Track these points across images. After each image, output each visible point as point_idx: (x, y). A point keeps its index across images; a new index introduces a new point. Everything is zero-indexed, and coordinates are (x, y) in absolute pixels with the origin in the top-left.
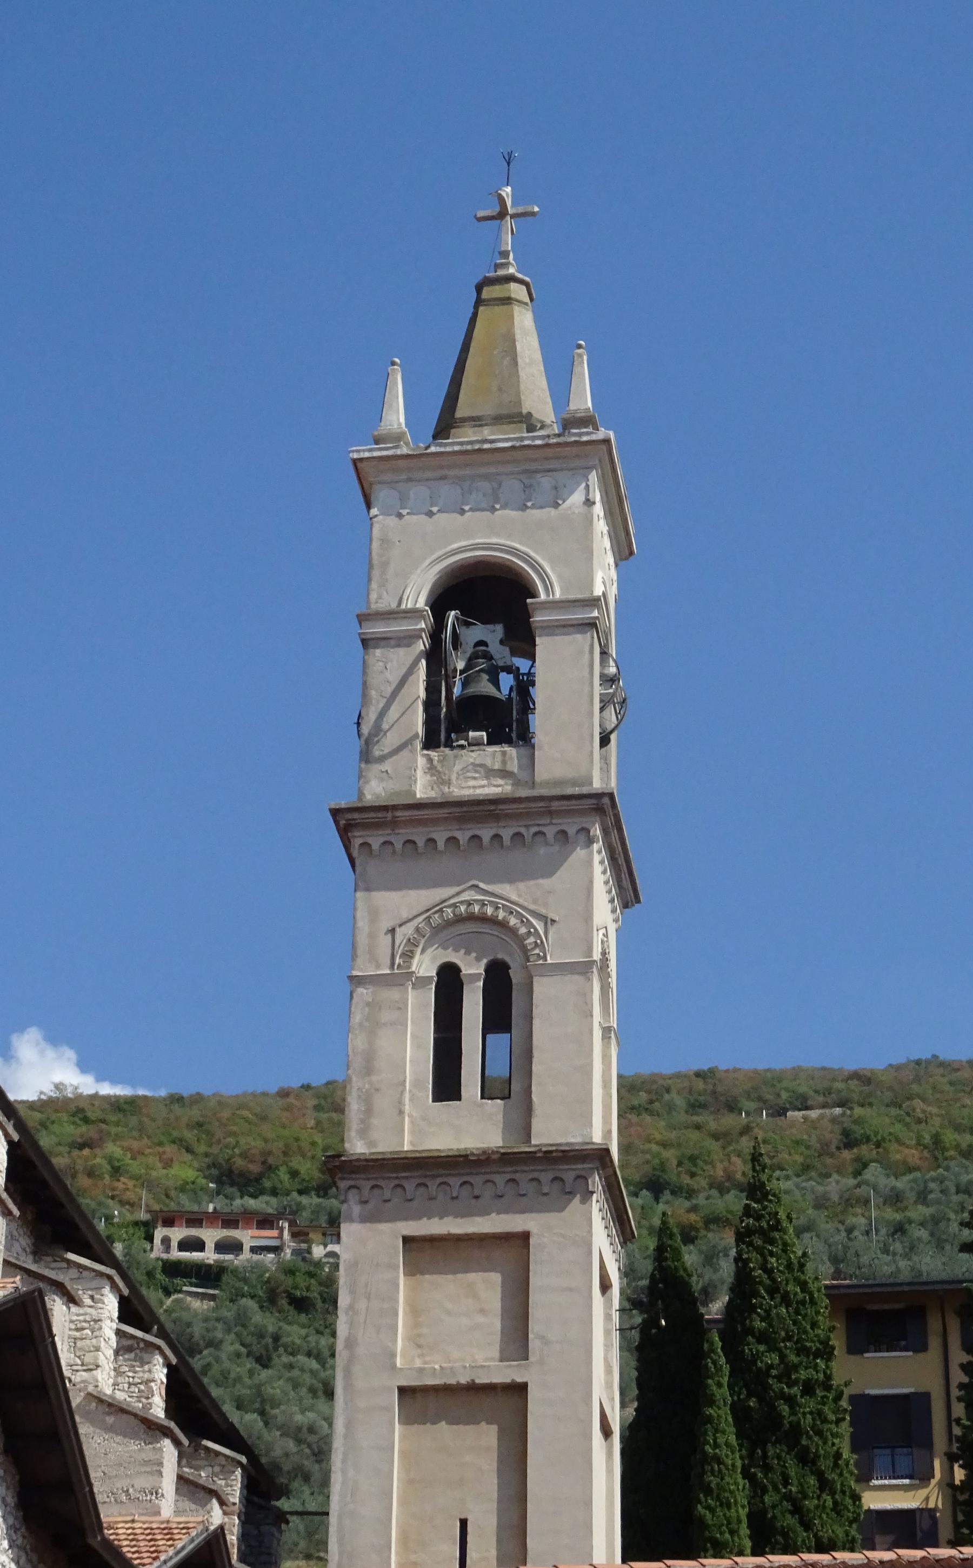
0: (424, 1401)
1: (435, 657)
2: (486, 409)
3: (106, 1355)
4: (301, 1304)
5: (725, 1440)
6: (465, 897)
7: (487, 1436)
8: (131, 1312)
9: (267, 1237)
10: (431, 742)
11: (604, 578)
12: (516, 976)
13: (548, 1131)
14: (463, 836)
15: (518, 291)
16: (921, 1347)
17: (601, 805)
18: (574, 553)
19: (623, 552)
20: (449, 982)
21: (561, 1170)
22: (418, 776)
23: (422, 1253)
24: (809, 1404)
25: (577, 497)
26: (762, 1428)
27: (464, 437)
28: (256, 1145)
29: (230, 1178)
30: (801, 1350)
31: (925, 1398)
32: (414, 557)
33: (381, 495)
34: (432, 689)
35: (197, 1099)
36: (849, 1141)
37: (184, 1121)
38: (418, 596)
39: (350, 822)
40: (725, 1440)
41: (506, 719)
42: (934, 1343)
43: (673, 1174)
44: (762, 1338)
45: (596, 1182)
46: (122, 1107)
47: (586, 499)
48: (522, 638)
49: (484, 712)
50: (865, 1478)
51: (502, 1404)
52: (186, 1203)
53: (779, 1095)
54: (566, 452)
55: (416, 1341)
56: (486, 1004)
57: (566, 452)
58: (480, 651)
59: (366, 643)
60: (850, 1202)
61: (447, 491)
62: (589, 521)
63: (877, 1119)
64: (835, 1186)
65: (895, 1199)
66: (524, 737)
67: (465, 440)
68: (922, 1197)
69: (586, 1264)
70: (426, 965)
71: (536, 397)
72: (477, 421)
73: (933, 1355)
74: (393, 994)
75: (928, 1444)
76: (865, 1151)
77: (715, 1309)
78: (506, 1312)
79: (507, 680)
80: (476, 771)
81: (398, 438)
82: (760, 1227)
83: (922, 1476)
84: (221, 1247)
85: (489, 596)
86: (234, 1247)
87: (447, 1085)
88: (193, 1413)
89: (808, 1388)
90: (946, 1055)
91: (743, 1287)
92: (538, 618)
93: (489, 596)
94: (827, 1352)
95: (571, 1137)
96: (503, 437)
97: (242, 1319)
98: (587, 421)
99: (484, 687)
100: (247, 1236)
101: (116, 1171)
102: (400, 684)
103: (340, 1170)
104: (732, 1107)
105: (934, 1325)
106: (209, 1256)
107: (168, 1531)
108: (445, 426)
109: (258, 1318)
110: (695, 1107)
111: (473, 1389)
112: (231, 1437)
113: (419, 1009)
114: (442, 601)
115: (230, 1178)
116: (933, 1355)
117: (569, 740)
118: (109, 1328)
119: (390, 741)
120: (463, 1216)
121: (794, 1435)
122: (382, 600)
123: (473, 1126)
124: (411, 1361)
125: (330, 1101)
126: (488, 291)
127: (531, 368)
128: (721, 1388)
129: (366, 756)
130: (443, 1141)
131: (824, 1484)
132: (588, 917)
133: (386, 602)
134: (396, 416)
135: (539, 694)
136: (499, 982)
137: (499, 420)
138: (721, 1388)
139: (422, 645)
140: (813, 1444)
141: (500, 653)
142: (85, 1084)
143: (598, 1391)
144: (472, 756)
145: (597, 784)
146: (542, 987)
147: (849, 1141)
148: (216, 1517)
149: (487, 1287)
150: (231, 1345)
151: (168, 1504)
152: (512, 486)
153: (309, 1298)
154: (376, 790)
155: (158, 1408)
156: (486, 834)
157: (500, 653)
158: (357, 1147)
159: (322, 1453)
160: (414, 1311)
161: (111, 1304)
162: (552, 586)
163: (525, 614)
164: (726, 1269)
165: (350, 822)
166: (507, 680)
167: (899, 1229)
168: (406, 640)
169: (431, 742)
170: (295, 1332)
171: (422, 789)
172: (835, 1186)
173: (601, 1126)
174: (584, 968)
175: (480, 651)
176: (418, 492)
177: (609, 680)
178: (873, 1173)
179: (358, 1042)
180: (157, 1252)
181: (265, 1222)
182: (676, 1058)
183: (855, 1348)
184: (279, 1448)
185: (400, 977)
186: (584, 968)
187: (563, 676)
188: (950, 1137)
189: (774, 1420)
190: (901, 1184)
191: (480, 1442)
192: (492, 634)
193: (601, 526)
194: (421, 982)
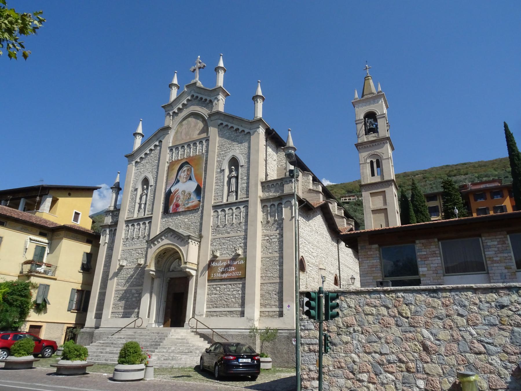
0: (374, 212)
1: (365, 124)
2: (367, 93)
3: (336, 210)
4: (359, 205)
5: (412, 213)
6: (372, 152)
7: (383, 215)
8: (338, 205)
9: (354, 198)
10: (366, 134)
11: (385, 111)
12: (380, 161)
13: (386, 178)
14: (371, 145)
15: (370, 78)
16: (437, 200)
17: (388, 139)
18: (381, 108)
19: (387, 107)
20: (372, 163)
21: (389, 183)
22: (365, 139)
23: (372, 194)
24: (423, 208)
25: (380, 102)
26: (417, 211)
27: (365, 97)
28: (351, 188)
29: (349, 192)
30: (421, 202)
31: (437, 206)
32: (361, 113)
33: (356, 106)
34: (365, 128)
35: (344, 183)
36: (424, 178)
37: (343, 186)
38: (362, 117)
39: (357, 145)
40: (412, 213)
41: (375, 130)
42: (438, 200)
43: (402, 185)
44: (416, 201)
45: (393, 184)
46: (335, 185)
47: (382, 102)
48: (376, 120)
49: (372, 130)
50: (431, 216)
51: (384, 211)
52: (344, 195)
53: (414, 174)
54: (379, 96)
55: (373, 205)
56: (377, 164)
57: (379, 96)
58: (371, 123)
59: (356, 124)
60: (425, 185)
61: (364, 104)
62: (382, 104)
63: (427, 175)
64: (422, 184)
65: (431, 184)
66: (377, 132)
67: (366, 97)
68: (434, 184)
69: (393, 193)
70: (368, 161)
71: (374, 90)
72: (367, 95)
73: (438, 201)
74: (364, 165)
75: (439, 212)
76: (426, 179)
77: (410, 199)
78: (386, 222)
79: (374, 126)
80: (372, 137)
81: (357, 99)
82: (414, 188)
83: (438, 216)
84: (349, 199)
85: (371, 116)
86: (350, 199)
87: (373, 174)
88: (347, 215)
89: (423, 206)
90: (435, 166)
91: (413, 196)
92: (377, 117)
93: (371, 116)
94: (424, 202)
95: (389, 179)
96: (370, 96)
97: (352, 207)
98: (381, 92)
99: (372, 127)
100: (351, 198)
101: (336, 192)
102: (361, 128)
103: (361, 186)
104: (409, 176)
105: (438, 197)
106: (347, 201)
107: (346, 228)
108: (363, 96)
109: (354, 207)
110: (404, 177)
111: (380, 209)
112: (352, 218)
113: (368, 166)
114: (365, 118)
115: (349, 192)
116: (438, 201)
117: (383, 131)
118: (336, 207)
119: (361, 135)
120: (369, 112)
121: (421, 212)
122: (357, 118)
123: (377, 179)
124: (372, 207)
125: (359, 181)
126: (366, 78)
127: (373, 87)
128: (411, 207)
129: (358, 137)
130: (373, 181)
131: (426, 217)
132: (388, 152)
133: (358, 119)
134: (357, 96)
135: (378, 126)
136: (378, 162)
137: (369, 94)
138: (411, 207)
139: (363, 123)
140: (424, 213)
141: (373, 122)
142: (331, 184)
143: (396, 208)
144: (371, 135)
145: (387, 136)
146: (383, 161)
147: (424, 178)
148: (351, 226)
149: (381, 198)
150: (351, 210)
151: (346, 226)
152: (372, 102)
153: (360, 204)
154: (360, 141)
155: (343, 215)
156: (374, 144)
157: (373, 122)
158: (363, 183)
159: (363, 221)
160: (372, 201)
161: (336, 204)
162: (378, 113)
163: (376, 117)
164: (410, 195)
165: (357, 145)
166: (374, 126)
167: (432, 188)
168: (362, 123)
169: (366, 134)
170: (358, 208)
171: (365, 140)
172: (422, 184)
173: (393, 177)
174: (388, 158)
175: (371, 123)
176: (360, 105)
177: (387, 123)
178: (427, 182)
179: (361, 171)
180: (342, 201)
181: (353, 196)
182: (401, 171)
183: (428, 201)
184: (358, 221)
185: (366, 163)
186: (388, 158)
187: (381, 124)
188: (437, 176)
189: (418, 210)
190: (431, 182)
191: (382, 216)
192: (372, 120)
193: (384, 105)
194: (368, 163)
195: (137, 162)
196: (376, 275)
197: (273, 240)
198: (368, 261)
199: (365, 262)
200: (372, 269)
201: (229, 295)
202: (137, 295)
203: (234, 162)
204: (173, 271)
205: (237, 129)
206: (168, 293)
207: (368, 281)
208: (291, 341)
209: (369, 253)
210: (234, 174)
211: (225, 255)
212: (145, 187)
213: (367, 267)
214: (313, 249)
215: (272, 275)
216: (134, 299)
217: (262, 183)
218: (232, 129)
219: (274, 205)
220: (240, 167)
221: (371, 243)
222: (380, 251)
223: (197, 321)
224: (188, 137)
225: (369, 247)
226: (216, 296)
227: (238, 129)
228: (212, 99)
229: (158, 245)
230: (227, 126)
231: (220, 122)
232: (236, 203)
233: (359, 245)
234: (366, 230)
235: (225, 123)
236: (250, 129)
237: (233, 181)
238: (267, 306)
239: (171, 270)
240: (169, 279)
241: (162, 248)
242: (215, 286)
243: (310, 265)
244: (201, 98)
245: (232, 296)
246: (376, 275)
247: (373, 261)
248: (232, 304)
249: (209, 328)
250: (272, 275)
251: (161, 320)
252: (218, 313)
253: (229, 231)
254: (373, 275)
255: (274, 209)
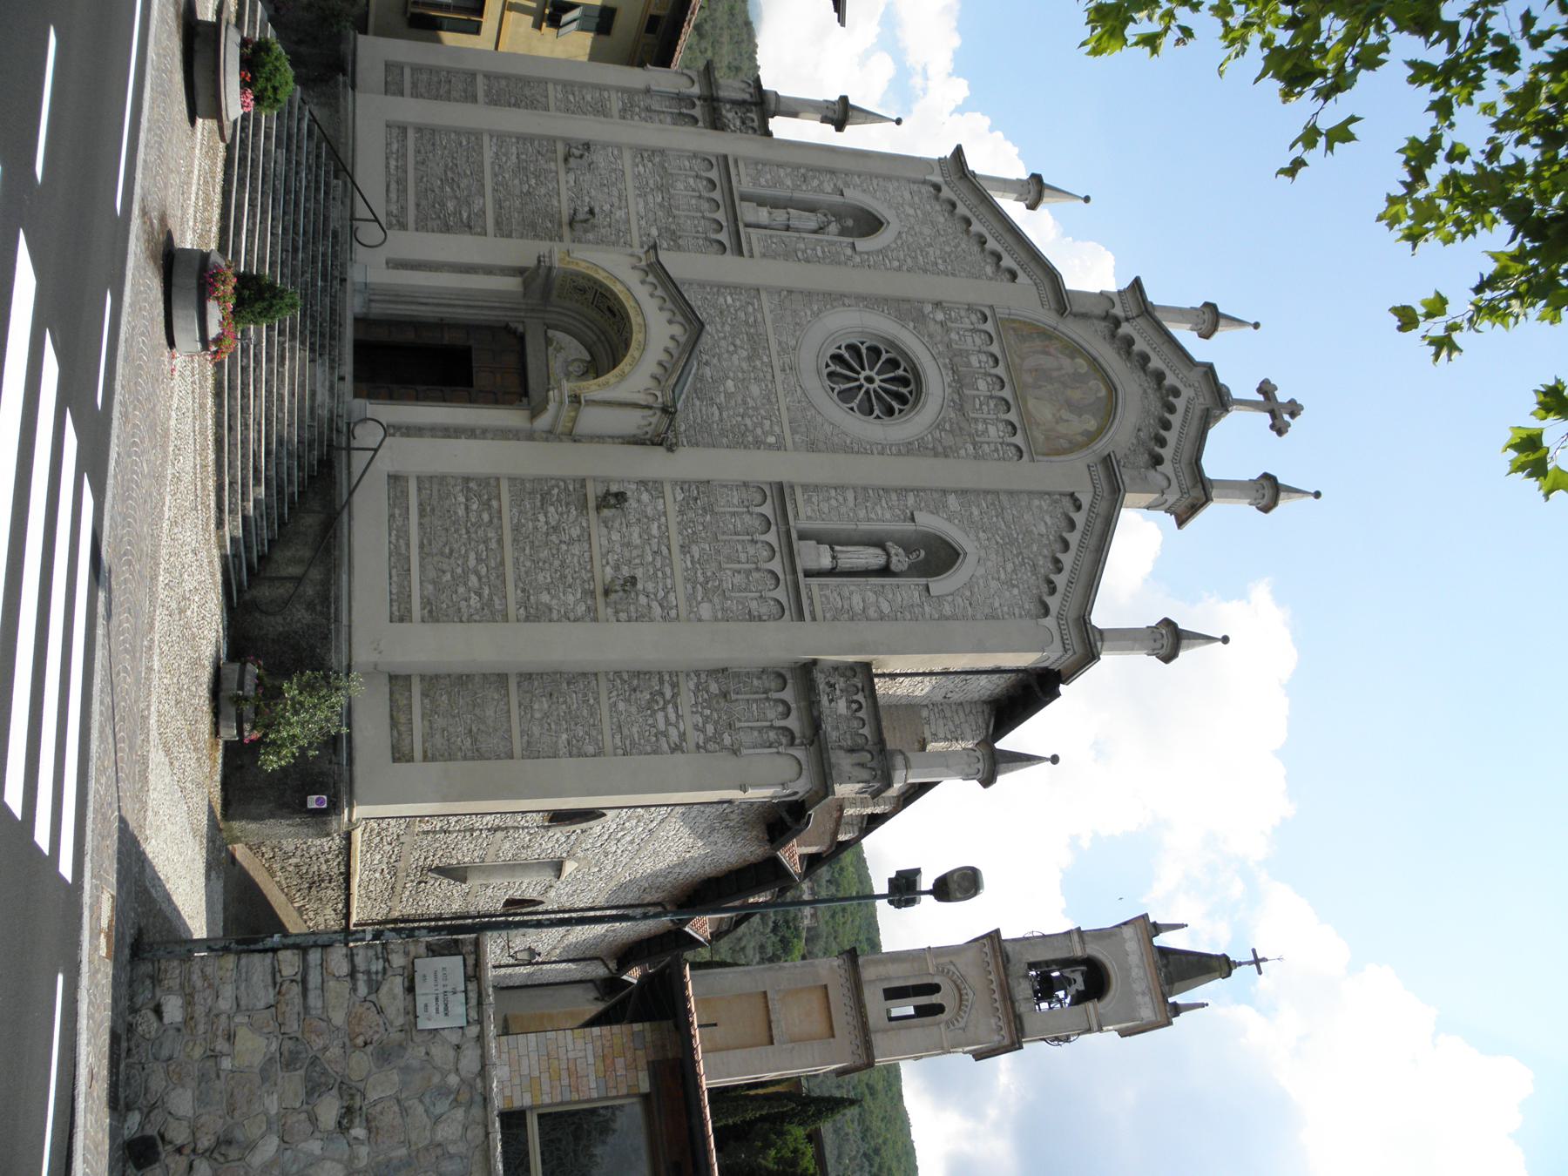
14: (994, 986)
195: (938, 188)
196: (546, 1087)
197: (660, 715)
198: (591, 1060)
199: (590, 1047)
200: (564, 1074)
201: (466, 557)
202: (465, 215)
203: (938, 557)
204: (548, 341)
205: (1058, 566)
206: (470, 328)
207: (525, 1062)
208: (267, 1167)
209: (620, 1062)
210: (900, 561)
211: (604, 542)
212: (850, 223)
213: (571, 1055)
214: (632, 842)
215: (538, 715)
216: (450, 205)
217: (867, 666)
218: (1058, 546)
219: (787, 714)
220: (923, 581)
221: (655, 1070)
222: (628, 1096)
223: (376, 450)
224: (1030, 380)
225: (642, 1063)
226: (461, 512)
227: (1060, 570)
228: (1167, 467)
229: (642, 292)
230: (1072, 525)
231: (1085, 500)
232: (794, 571)
233: (647, 1025)
234: (707, 918)
235: (1080, 518)
236: (1059, 617)
237: (870, 557)
238: (426, 723)
239: (551, 333)
240: (520, 329)
241: (629, 305)
242: (495, 503)
243: (573, 837)
244: (1167, 425)
245: (459, 571)
246: (546, 1087)
247: (592, 1078)
248: (432, 574)
249: (351, 493)
250: (538, 715)
251: (377, 309)
252: (399, 522)
253: (695, 549)
254: (545, 1078)
255: (771, 714)
